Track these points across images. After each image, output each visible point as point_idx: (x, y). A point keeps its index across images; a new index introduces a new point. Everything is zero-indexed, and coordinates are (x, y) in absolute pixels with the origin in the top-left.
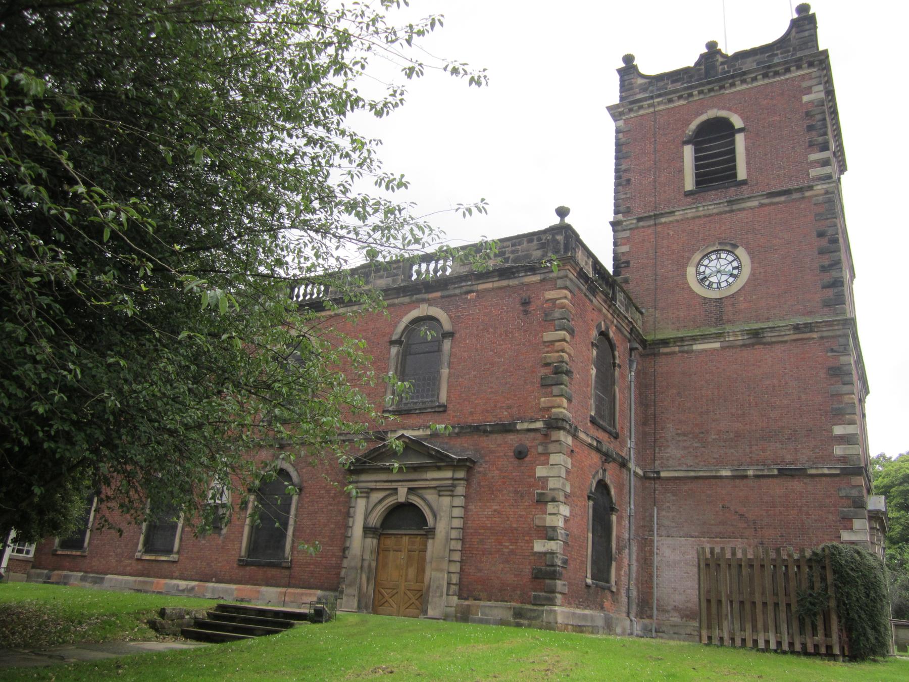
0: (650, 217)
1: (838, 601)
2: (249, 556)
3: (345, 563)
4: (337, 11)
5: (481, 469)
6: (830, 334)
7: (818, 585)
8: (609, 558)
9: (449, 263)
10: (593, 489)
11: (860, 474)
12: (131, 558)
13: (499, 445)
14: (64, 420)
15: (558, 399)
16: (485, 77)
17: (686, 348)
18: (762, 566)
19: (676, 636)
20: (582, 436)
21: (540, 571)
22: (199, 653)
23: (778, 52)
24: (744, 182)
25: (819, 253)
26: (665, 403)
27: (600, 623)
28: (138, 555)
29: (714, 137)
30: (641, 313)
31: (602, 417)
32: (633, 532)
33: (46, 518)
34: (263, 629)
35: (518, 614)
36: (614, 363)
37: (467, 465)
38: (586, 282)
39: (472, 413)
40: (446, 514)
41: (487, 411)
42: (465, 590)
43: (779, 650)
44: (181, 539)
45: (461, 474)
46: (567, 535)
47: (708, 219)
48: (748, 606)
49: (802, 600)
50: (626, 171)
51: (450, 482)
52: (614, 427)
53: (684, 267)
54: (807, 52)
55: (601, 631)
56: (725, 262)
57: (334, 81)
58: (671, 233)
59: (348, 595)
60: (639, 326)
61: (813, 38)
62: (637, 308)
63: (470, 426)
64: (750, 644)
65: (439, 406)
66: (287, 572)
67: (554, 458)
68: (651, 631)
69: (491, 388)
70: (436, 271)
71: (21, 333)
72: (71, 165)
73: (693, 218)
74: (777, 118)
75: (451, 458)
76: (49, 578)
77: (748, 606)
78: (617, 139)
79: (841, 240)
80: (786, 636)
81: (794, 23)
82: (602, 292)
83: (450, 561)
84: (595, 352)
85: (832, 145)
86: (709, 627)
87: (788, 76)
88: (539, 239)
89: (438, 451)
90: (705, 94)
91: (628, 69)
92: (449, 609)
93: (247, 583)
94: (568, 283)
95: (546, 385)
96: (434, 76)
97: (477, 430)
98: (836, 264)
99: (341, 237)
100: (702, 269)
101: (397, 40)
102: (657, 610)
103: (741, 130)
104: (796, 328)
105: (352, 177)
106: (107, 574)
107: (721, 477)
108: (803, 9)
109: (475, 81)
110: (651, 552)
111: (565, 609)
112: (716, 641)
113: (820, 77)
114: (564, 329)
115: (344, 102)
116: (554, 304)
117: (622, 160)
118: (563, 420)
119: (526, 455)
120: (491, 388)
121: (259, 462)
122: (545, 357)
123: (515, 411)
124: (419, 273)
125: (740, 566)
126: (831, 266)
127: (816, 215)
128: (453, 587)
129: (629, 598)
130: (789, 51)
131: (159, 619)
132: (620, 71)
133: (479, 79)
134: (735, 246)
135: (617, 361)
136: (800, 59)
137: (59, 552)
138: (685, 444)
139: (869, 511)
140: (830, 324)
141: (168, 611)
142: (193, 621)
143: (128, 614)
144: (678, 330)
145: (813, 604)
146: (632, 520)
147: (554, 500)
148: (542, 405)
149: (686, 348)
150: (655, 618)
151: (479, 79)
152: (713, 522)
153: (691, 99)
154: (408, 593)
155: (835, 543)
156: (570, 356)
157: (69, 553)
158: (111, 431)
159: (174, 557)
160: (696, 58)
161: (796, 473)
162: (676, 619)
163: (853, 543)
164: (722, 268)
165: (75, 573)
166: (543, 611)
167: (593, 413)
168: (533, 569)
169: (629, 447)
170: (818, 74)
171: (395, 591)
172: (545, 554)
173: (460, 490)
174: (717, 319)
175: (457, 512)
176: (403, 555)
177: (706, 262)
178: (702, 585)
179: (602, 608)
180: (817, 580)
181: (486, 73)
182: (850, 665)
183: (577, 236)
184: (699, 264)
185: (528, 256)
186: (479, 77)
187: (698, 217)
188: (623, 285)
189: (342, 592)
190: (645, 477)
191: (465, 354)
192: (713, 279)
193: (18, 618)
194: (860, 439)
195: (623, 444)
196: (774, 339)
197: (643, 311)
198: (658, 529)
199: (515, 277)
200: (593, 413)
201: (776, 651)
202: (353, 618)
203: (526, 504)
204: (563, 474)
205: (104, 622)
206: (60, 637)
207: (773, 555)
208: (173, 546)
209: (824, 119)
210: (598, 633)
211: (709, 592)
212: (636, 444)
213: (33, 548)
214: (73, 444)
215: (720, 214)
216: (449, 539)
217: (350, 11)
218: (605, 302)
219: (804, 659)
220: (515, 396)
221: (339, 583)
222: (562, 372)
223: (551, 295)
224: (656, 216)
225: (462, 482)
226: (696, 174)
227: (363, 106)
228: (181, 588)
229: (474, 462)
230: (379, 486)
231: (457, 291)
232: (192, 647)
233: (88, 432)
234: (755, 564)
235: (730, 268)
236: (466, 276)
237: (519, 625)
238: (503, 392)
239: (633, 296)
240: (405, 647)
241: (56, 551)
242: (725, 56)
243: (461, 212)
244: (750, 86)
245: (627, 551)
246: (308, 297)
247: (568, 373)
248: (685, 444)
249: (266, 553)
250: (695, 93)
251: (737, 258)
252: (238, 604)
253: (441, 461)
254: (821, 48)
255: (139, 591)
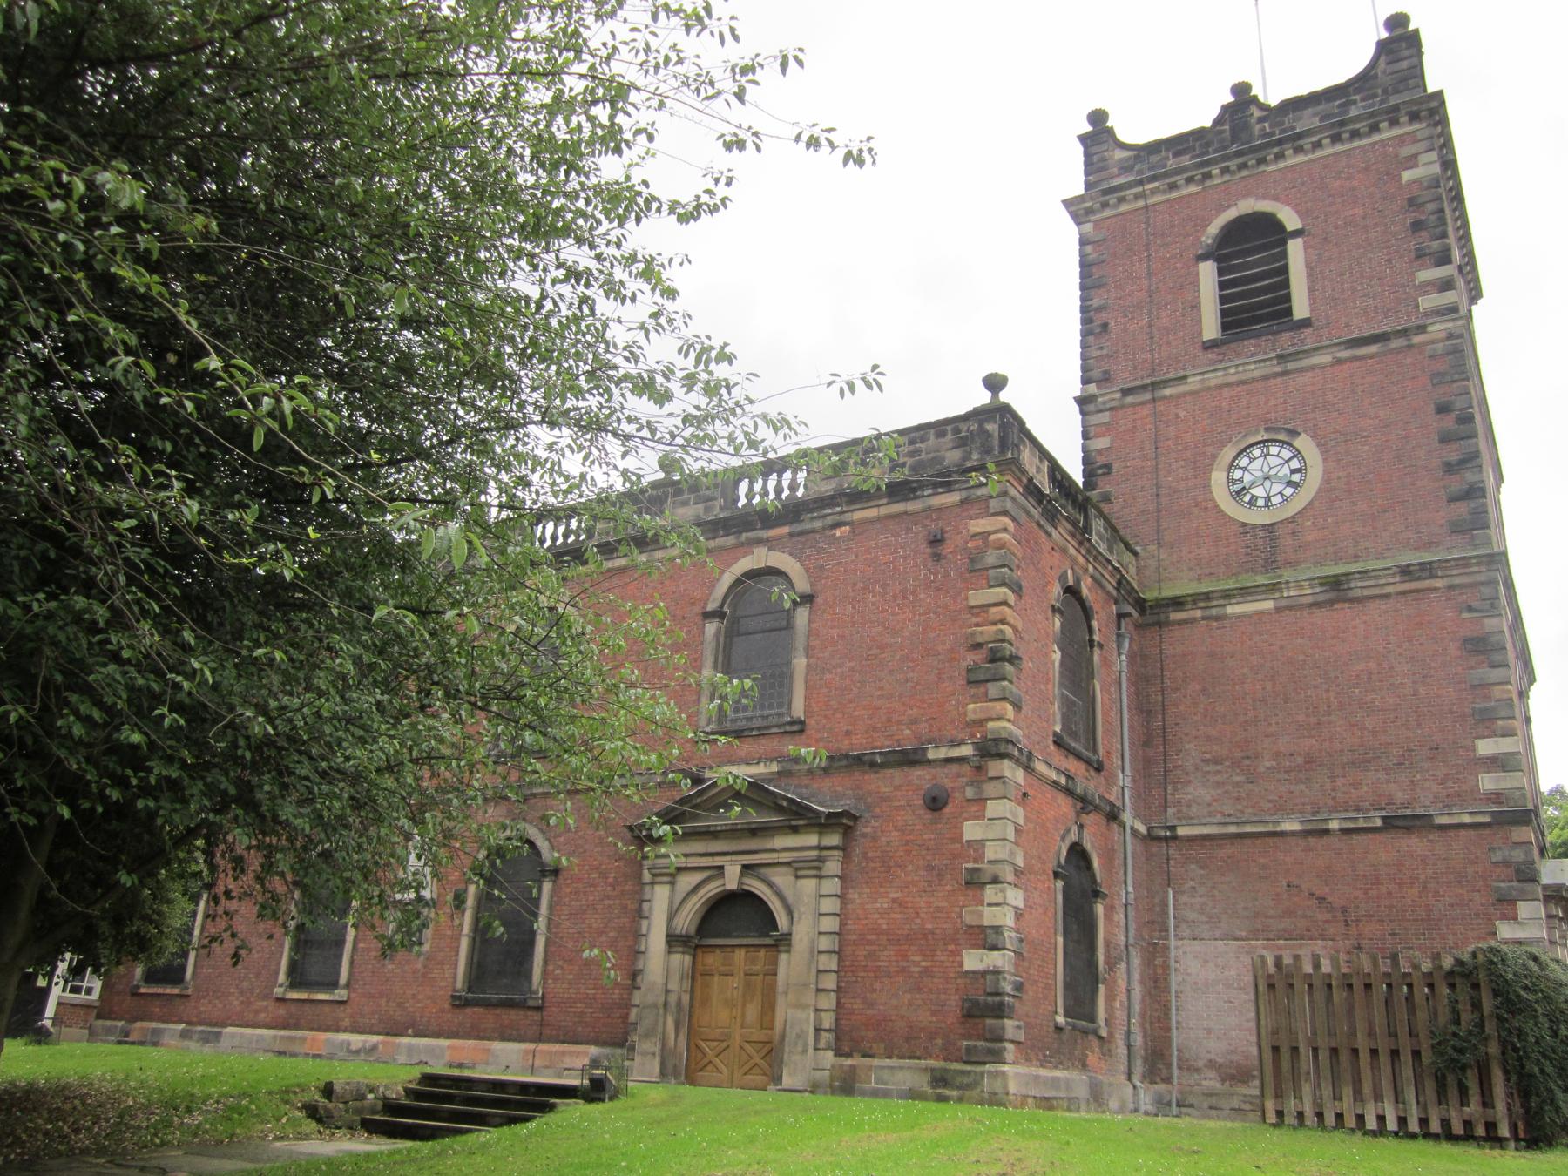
0: (1144, 387)
1: (1504, 1043)
2: (469, 990)
3: (637, 998)
4: (604, 45)
5: (869, 830)
6: (1465, 580)
7: (1467, 1017)
8: (1095, 980)
9: (802, 476)
10: (1063, 861)
11: (1527, 822)
12: (266, 997)
13: (897, 788)
14: (169, 760)
15: (998, 705)
16: (870, 150)
17: (1214, 612)
18: (1368, 986)
19: (1213, 1112)
20: (1040, 767)
21: (975, 1003)
22: (397, 1157)
23: (1357, 97)
24: (1306, 323)
25: (1442, 441)
26: (1182, 708)
27: (1082, 1092)
28: (278, 991)
29: (1252, 241)
30: (1135, 554)
31: (1073, 735)
32: (1132, 933)
33: (127, 931)
34: (501, 1115)
35: (941, 1079)
36: (1091, 642)
37: (843, 822)
38: (1040, 502)
39: (848, 733)
40: (809, 907)
41: (874, 728)
42: (845, 1040)
43: (1403, 1133)
44: (352, 963)
45: (834, 839)
46: (1021, 940)
47: (1245, 387)
48: (1345, 1056)
49: (1439, 1043)
50: (1100, 309)
51: (815, 853)
52: (1095, 751)
53: (1206, 471)
54: (1407, 96)
55: (1083, 1106)
56: (1276, 460)
57: (609, 168)
58: (1182, 414)
59: (644, 1054)
60: (1131, 575)
61: (1417, 72)
62: (1127, 545)
63: (847, 756)
64: (1350, 1122)
65: (792, 723)
66: (536, 1016)
67: (993, 808)
68: (1169, 1104)
69: (881, 689)
70: (779, 490)
71: (101, 613)
72: (194, 323)
73: (1220, 387)
74: (1359, 211)
75: (815, 811)
76: (127, 1035)
77: (1345, 1056)
78: (1083, 256)
79: (1478, 418)
80: (1414, 1107)
81: (1382, 46)
82: (1067, 519)
83: (818, 990)
84: (1058, 623)
85: (1456, 254)
86: (1279, 1095)
87: (1375, 138)
88: (957, 431)
89: (792, 801)
90: (1233, 173)
91: (1098, 135)
92: (819, 1074)
93: (467, 1036)
94: (1009, 505)
95: (975, 681)
96: (782, 154)
97: (860, 762)
98: (1471, 459)
99: (628, 437)
100: (1237, 474)
101: (719, 93)
102: (1180, 1068)
103: (1297, 233)
104: (1406, 572)
105: (647, 335)
106: (225, 1025)
107: (1283, 834)
108: (1397, 22)
109: (854, 158)
110: (1166, 968)
111: (1021, 1069)
112: (1290, 1119)
113: (1431, 137)
114: (1003, 584)
115: (624, 202)
116: (985, 540)
117: (1093, 292)
118: (1008, 741)
119: (945, 804)
120: (881, 689)
121: (492, 825)
122: (973, 634)
123: (923, 728)
124: (750, 494)
125: (1330, 986)
126: (1462, 462)
127: (1434, 375)
128: (824, 1034)
129: (1129, 1047)
130: (1375, 96)
131: (323, 1101)
132: (1083, 139)
133: (859, 155)
134: (1294, 433)
135: (1096, 638)
136: (1396, 108)
137: (143, 990)
138: (1218, 778)
139: (1545, 887)
140: (1464, 562)
141: (337, 1087)
142: (380, 1103)
143: (270, 1093)
144: (1199, 580)
145: (1461, 1051)
146: (1131, 913)
147: (995, 880)
148: (970, 716)
149: (1214, 612)
150: (1175, 1081)
151: (859, 155)
152: (1271, 912)
153: (1208, 183)
154: (747, 1046)
155: (1493, 943)
156: (1015, 630)
157: (160, 991)
158: (250, 777)
159: (340, 994)
160: (1214, 112)
161: (1416, 824)
162: (1212, 1083)
163: (1519, 942)
164: (1273, 472)
165: (171, 1026)
166: (982, 1074)
167: (1058, 729)
168: (964, 1001)
169: (1122, 785)
170: (1427, 132)
171: (724, 1045)
172: (984, 974)
173: (833, 866)
174: (1266, 560)
175: (830, 905)
176: (735, 982)
177: (1244, 462)
178: (1263, 1022)
179: (1084, 1066)
180: (1464, 1007)
181: (872, 144)
182: (1529, 1154)
183: (1021, 423)
184: (1232, 465)
185: (937, 460)
186: (861, 151)
187: (1228, 385)
188: (1102, 505)
189: (632, 1048)
190: (1151, 837)
191: (835, 632)
192: (1258, 491)
193: (84, 1104)
194: (1524, 760)
195: (1110, 781)
196: (1366, 592)
197: (1138, 549)
198: (1176, 927)
199: (916, 498)
200: (1058, 729)
201: (1396, 1134)
202: (658, 1093)
203: (948, 888)
204: (1011, 835)
205: (231, 1108)
206: (156, 1135)
207: (1385, 967)
208: (338, 974)
209: (1442, 210)
210: (1078, 1110)
211: (1275, 1033)
212: (1134, 780)
213: (97, 985)
214: (185, 801)
215: (1266, 378)
216: (815, 953)
217: (626, 43)
218: (1073, 535)
219: (1446, 1147)
220: (922, 701)
221: (626, 1033)
222: (1003, 659)
223: (979, 525)
224: (1155, 386)
225: (836, 853)
226: (1222, 311)
227: (659, 210)
228: (353, 1047)
229: (855, 818)
230: (693, 862)
231: (818, 524)
232: (383, 1147)
233: (209, 780)
234: (1354, 981)
235: (1286, 470)
236: (832, 497)
237: (942, 1099)
238: (901, 696)
239: (1119, 527)
240: (752, 1140)
241: (138, 987)
242: (1264, 107)
243: (835, 388)
244: (1310, 157)
245: (1123, 966)
246: (572, 538)
247: (1013, 659)
248: (1218, 778)
249: (499, 980)
250: (1215, 171)
251: (1298, 454)
252: (456, 1072)
253: (797, 816)
254: (1430, 90)
255: (280, 1053)
